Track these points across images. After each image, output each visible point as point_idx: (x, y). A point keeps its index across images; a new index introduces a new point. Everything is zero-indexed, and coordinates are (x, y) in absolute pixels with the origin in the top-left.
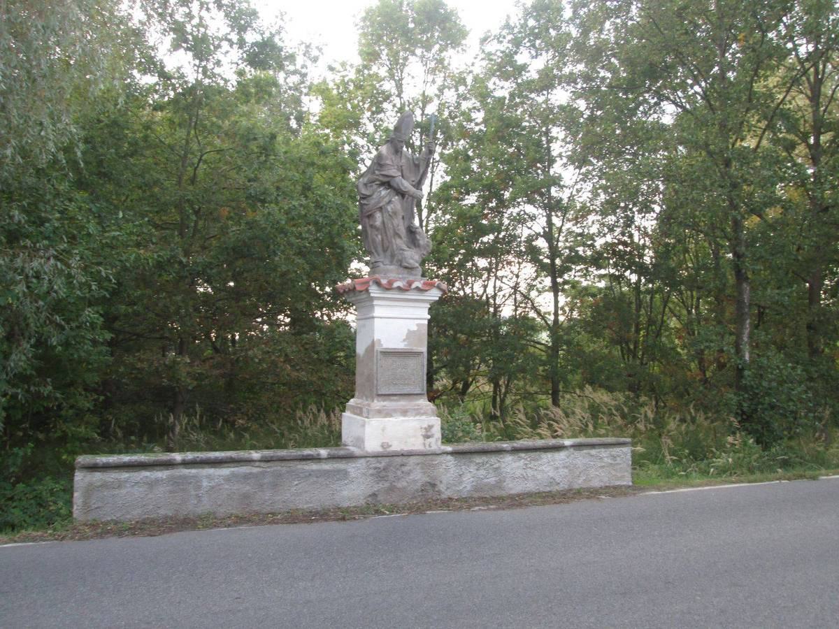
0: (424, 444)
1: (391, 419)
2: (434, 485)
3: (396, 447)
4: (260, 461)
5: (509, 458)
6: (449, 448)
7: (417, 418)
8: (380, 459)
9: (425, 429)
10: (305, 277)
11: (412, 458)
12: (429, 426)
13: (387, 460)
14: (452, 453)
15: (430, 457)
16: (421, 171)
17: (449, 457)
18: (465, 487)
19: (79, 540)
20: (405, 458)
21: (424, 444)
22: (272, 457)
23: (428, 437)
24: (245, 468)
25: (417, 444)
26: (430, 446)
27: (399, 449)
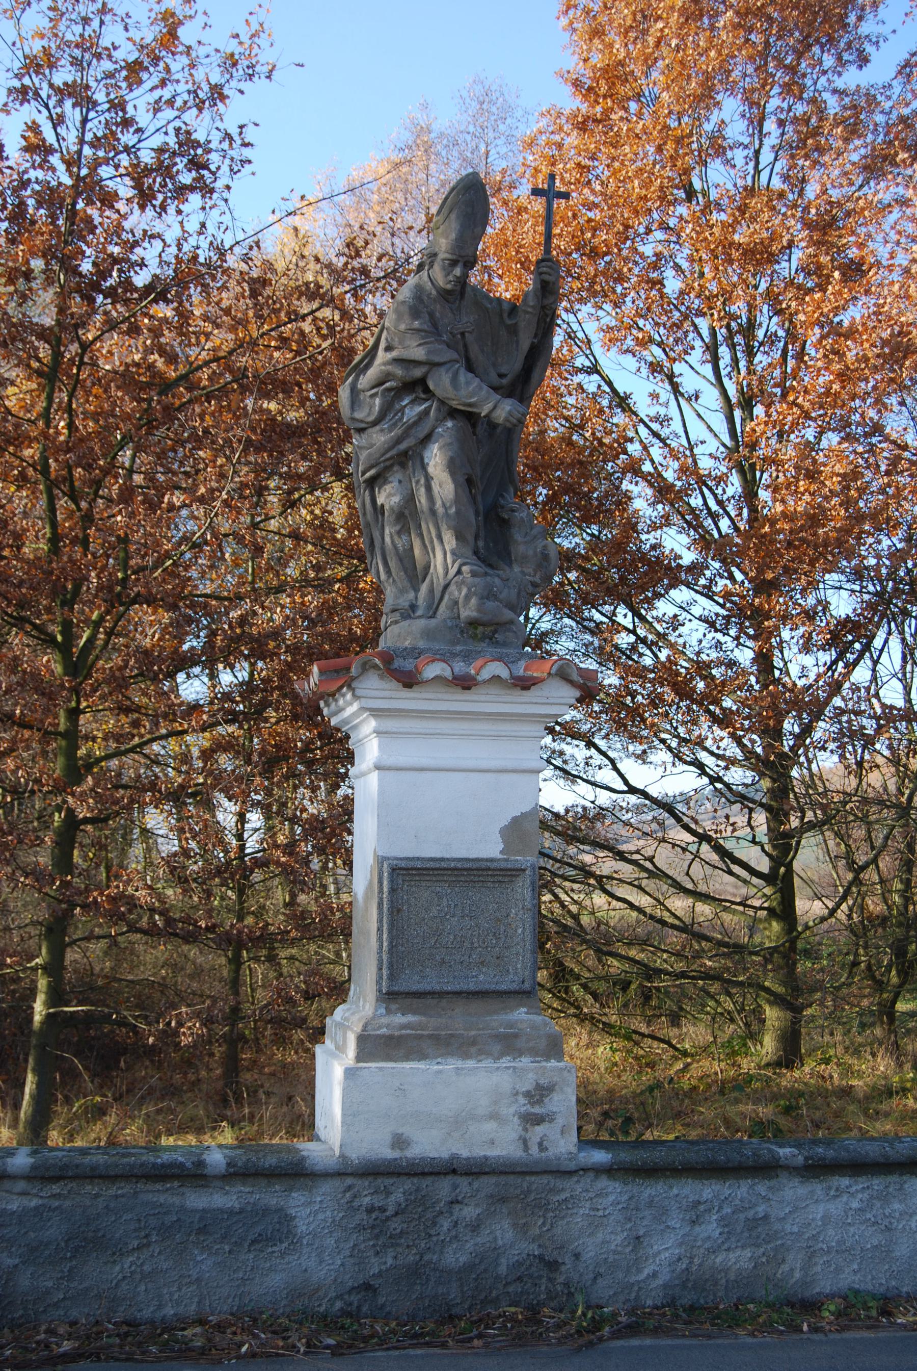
0: (525, 1143)
1: (421, 1065)
2: (554, 1266)
3: (429, 1144)
4: (28, 1178)
5: (793, 1190)
6: (600, 1157)
7: (505, 1061)
8: (381, 1182)
9: (528, 1094)
10: (644, 192)
11: (484, 1179)
12: (539, 1087)
13: (408, 1184)
14: (609, 1171)
15: (545, 1179)
16: (525, 344)
17: (603, 1182)
18: (655, 1275)
19: (337, 1351)
20: (429, 1180)
21: (525, 1143)
22: (66, 1167)
23: (538, 1120)
24: (329, 1073)
25: (500, 1140)
26: (541, 1146)
27: (445, 1155)
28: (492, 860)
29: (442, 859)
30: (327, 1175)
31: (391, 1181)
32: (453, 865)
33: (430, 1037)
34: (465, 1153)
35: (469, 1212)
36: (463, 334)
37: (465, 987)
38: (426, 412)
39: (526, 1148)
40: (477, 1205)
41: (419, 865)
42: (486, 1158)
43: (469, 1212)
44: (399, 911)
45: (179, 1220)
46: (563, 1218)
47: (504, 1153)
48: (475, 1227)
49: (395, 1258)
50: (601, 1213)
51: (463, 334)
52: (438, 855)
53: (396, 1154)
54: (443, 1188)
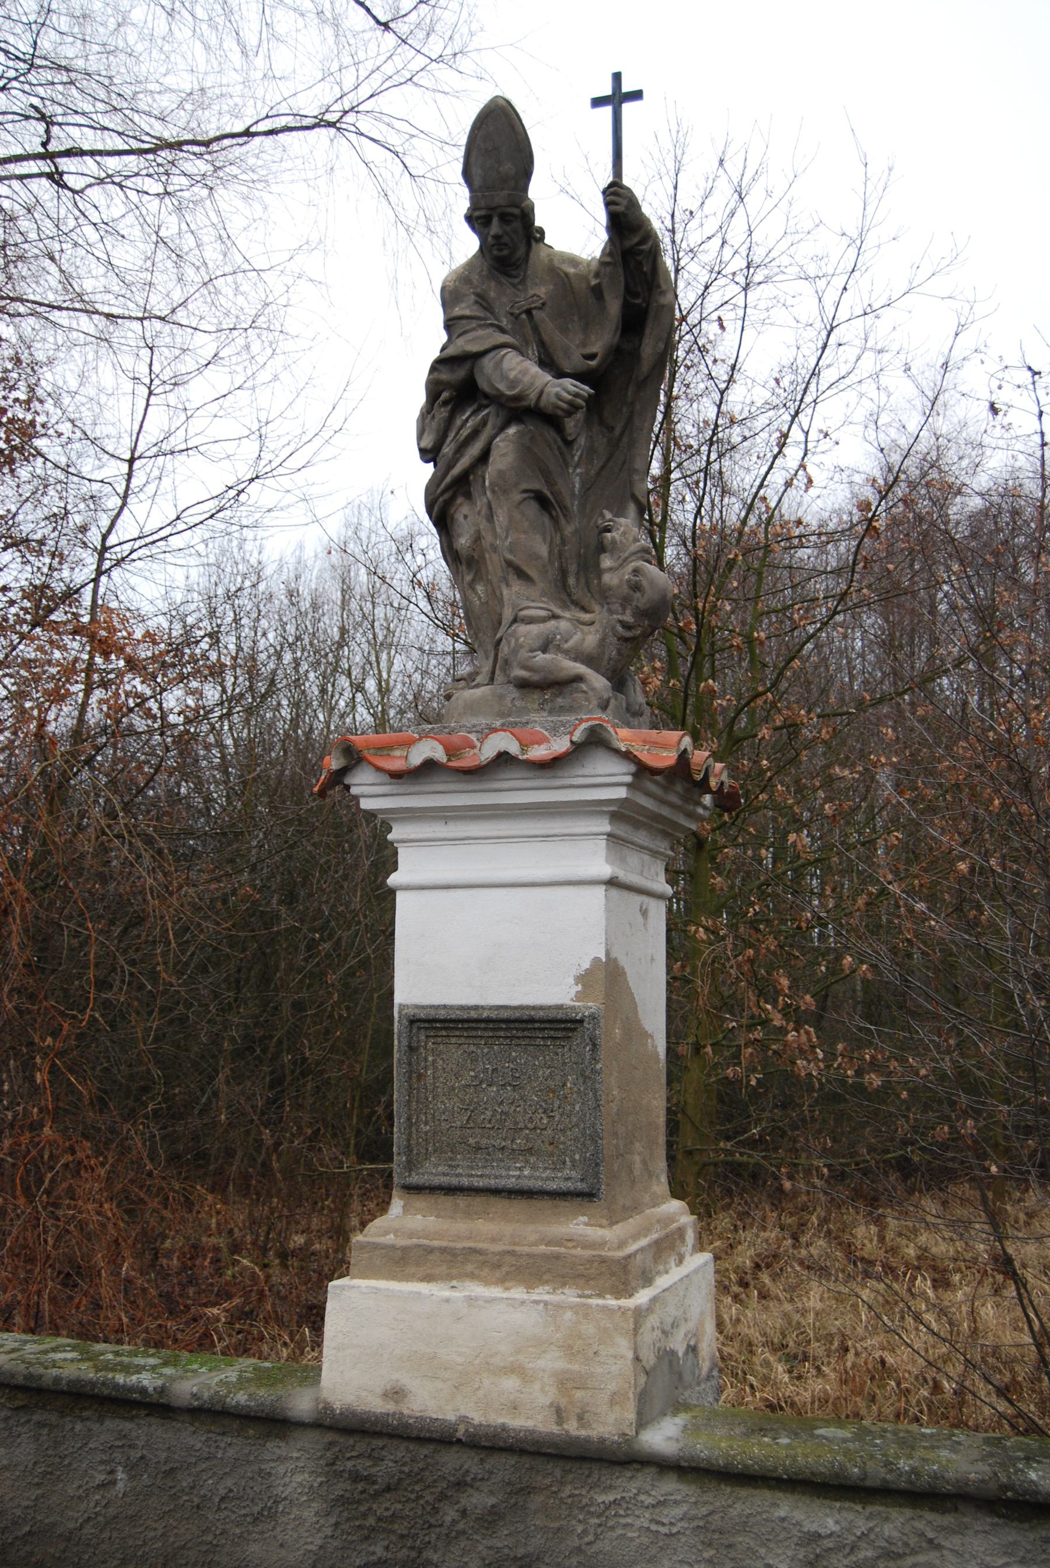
1: (424, 1288)
17: (670, 1486)
25: (523, 1406)
28: (560, 1007)
29: (476, 1008)
30: (301, 1425)
31: (380, 1443)
32: (485, 1015)
33: (443, 1250)
34: (477, 1418)
35: (479, 1500)
36: (529, 312)
37: (502, 1183)
38: (484, 423)
39: (560, 1419)
40: (492, 1493)
41: (505, 1015)
42: (504, 1428)
43: (479, 1500)
44: (420, 1077)
45: (142, 1457)
46: (612, 1528)
47: (529, 1424)
48: (491, 1519)
49: (387, 1548)
50: (664, 1530)
51: (529, 312)
52: (472, 1002)
53: (390, 1407)
54: (451, 1461)
